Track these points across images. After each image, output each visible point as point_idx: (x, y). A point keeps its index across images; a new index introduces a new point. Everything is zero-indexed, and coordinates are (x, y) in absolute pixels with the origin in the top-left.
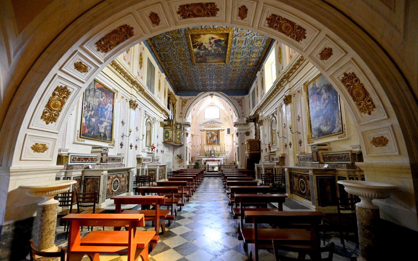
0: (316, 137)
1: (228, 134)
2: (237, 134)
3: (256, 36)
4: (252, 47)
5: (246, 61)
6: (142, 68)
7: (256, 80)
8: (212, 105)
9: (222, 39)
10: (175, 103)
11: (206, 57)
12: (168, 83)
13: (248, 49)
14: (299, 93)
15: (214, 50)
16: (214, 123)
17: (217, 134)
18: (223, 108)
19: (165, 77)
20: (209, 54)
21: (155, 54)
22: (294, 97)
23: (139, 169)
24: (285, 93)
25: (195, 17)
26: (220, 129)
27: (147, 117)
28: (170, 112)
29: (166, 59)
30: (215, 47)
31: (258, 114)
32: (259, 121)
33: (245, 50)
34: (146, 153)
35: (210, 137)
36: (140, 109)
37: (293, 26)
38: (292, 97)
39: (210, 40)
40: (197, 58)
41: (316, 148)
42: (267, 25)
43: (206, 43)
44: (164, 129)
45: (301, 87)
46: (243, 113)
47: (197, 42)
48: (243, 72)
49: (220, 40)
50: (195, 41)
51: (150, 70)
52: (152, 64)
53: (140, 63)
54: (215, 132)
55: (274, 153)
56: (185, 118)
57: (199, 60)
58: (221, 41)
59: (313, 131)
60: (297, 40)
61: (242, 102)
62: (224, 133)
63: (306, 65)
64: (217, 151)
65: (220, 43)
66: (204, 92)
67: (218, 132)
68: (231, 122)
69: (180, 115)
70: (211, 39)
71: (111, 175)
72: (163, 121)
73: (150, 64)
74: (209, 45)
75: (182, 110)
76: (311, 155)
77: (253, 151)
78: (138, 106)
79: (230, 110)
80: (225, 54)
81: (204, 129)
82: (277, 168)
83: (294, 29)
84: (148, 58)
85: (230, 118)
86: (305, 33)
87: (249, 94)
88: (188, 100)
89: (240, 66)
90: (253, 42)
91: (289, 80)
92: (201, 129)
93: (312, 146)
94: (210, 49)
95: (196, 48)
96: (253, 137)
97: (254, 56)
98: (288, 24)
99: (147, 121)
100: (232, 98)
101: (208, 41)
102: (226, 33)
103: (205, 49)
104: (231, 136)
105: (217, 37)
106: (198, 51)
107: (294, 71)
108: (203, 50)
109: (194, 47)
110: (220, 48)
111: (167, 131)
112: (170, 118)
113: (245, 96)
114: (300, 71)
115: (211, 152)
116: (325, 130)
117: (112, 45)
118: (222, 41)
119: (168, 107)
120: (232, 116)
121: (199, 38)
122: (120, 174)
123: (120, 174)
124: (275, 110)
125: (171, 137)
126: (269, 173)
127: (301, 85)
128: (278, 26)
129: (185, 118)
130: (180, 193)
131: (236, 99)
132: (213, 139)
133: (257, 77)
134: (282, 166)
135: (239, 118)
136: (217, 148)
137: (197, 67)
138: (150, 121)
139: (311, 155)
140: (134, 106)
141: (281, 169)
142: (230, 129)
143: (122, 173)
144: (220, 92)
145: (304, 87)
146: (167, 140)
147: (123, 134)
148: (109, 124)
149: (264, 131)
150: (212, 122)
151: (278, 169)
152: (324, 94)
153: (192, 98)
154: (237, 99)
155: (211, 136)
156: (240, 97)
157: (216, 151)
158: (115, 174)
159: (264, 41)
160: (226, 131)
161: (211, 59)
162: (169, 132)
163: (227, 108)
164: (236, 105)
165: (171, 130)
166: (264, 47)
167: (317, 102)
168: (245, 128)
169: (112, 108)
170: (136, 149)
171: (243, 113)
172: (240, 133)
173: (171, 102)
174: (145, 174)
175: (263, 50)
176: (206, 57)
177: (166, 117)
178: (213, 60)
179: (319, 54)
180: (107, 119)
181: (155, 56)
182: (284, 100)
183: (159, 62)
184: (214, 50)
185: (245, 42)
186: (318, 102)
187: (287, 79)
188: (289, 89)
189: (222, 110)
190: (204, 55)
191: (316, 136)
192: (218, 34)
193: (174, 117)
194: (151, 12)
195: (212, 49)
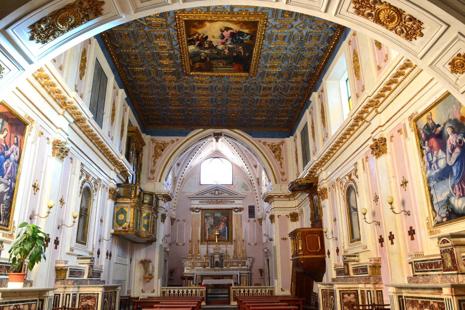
0: (445, 220)
5: (291, 73)
6: (84, 78)
7: (310, 107)
8: (217, 155)
9: (246, 31)
11: (212, 62)
12: (129, 108)
14: (401, 133)
15: (228, 50)
16: (221, 194)
17: (226, 218)
18: (239, 162)
19: (125, 96)
20: (219, 56)
21: (110, 52)
22: (391, 141)
23: (60, 295)
24: (372, 133)
27: (84, 178)
28: (130, 168)
29: (130, 62)
30: (230, 44)
31: (316, 176)
32: (318, 190)
34: (76, 257)
35: (212, 224)
36: (71, 159)
37: (401, 16)
38: (388, 142)
39: (222, 31)
40: (194, 63)
41: (448, 242)
42: (353, 10)
43: (213, 37)
44: (115, 203)
45: (403, 123)
46: (283, 174)
47: (197, 35)
49: (241, 33)
50: (192, 33)
51: (98, 83)
52: (102, 70)
53: (80, 69)
54: (222, 214)
55: (356, 258)
56: (160, 181)
57: (197, 66)
58: (244, 35)
59: (436, 208)
60: (408, 39)
61: (280, 150)
62: (241, 215)
63: (409, 84)
65: (241, 38)
66: (201, 130)
67: (227, 212)
68: (257, 191)
69: (150, 175)
70: (225, 30)
71: (6, 303)
72: (115, 187)
73: (99, 72)
74: (220, 40)
75: (154, 165)
76: (440, 257)
77: (310, 253)
78: (69, 153)
79: (254, 168)
80: (250, 57)
81: (199, 206)
82: (366, 290)
83: (401, 20)
84: (97, 59)
85: (255, 185)
86: (421, 28)
87: (294, 135)
88: (168, 144)
91: (379, 110)
92: (192, 206)
93: (439, 238)
94: (220, 47)
95: (195, 44)
96: (305, 222)
97: (305, 63)
98: (391, 12)
99: (82, 185)
100: (260, 142)
101: (218, 34)
103: (211, 46)
105: (235, 28)
106: (197, 50)
107: (387, 93)
108: (206, 49)
109: (191, 42)
110: (240, 47)
112: (130, 181)
113: (286, 139)
114: (400, 93)
116: (460, 205)
117: (60, 30)
118: (246, 35)
119: (128, 157)
121: (201, 28)
122: (24, 301)
123: (24, 301)
124: (353, 167)
126: (350, 302)
127: (405, 119)
128: (373, 13)
129: (160, 181)
130: (343, 269)
131: (269, 145)
133: (311, 102)
134: (377, 286)
135: (276, 183)
136: (228, 249)
138: (89, 186)
139: (440, 257)
140: (62, 152)
141: (375, 293)
143: (28, 301)
145: (410, 124)
146: (120, 228)
147: (33, 212)
148: (8, 189)
149: (333, 209)
150: (217, 193)
151: (368, 291)
152: (450, 136)
153: (177, 140)
154: (270, 144)
155: (214, 223)
156: (276, 141)
158: (13, 302)
160: (245, 213)
163: (249, 164)
164: (269, 156)
167: (438, 151)
169: (18, 154)
170: (56, 248)
171: (283, 174)
172: (279, 216)
173: (134, 148)
174: (72, 305)
176: (212, 62)
177: (122, 178)
178: (225, 67)
179: (448, 63)
180: (5, 177)
181: (111, 56)
182: (371, 147)
183: (116, 67)
184: (229, 49)
186: (440, 151)
187: (375, 108)
188: (380, 126)
189: (237, 166)
190: (208, 59)
191: (444, 217)
192: (236, 23)
193: (138, 180)
195: (226, 48)
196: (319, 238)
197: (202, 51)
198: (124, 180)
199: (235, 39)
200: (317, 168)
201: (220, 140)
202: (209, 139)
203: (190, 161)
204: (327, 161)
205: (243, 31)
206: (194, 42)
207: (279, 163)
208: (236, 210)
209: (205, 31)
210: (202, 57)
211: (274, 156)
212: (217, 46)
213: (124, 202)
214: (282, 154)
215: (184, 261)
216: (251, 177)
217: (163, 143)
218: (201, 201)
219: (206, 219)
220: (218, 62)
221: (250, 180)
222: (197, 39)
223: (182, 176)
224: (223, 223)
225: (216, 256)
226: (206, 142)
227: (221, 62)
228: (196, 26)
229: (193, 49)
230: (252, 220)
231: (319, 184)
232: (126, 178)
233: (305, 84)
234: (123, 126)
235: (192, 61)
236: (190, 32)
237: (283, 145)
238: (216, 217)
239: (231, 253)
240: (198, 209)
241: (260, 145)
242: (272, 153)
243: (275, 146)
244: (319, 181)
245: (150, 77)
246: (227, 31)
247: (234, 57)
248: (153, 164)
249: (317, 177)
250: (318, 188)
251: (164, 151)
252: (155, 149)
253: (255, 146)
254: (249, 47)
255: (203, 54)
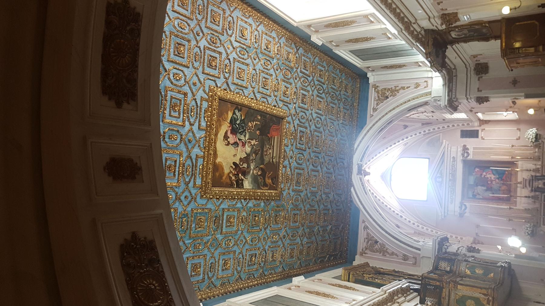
1: (477, 137)
2: (481, 100)
3: (233, 39)
4: (255, 50)
8: (385, 177)
9: (230, 114)
10: (373, 268)
11: (265, 162)
12: (318, 276)
13: (257, 60)
15: (252, 140)
17: (477, 170)
19: (302, 278)
20: (259, 152)
25: (137, 67)
26: (460, 158)
31: (423, 32)
33: (259, 67)
35: (485, 188)
39: (228, 144)
47: (231, 175)
48: (310, 79)
49: (233, 122)
52: (266, 299)
56: (419, 250)
58: (235, 118)
61: (385, 89)
62: (474, 148)
64: (536, 170)
65: (238, 122)
66: (352, 189)
74: (240, 148)
75: (396, 255)
79: (407, 129)
84: (251, 303)
87: (365, 70)
88: (368, 234)
89: (294, 84)
90: (245, 47)
94: (248, 149)
95: (242, 180)
96: (491, 49)
102: (219, 103)
103: (246, 160)
104: (487, 127)
105: (225, 127)
106: (249, 177)
108: (249, 167)
109: (240, 184)
111: (458, 301)
112: (416, 287)
115: (537, 189)
120: (423, 124)
121: (223, 169)
125: (479, 290)
129: (419, 250)
131: (377, 104)
132: (492, 181)
137: (287, 190)
142: (462, 131)
144: (356, 146)
153: (364, 222)
154: (376, 102)
155: (482, 186)
156: (372, 95)
157: (533, 174)
159: (246, 22)
160: (471, 143)
161: (271, 151)
162: (460, 294)
165: (456, 287)
166: (257, 24)
168: (461, 76)
172: (479, 90)
175: (265, 26)
176: (265, 162)
178: (273, 146)
184: (251, 139)
185: (243, 63)
194: (104, 169)
196: (518, 24)
197: (251, 172)
198: (415, 294)
199: (240, 129)
200: (412, 29)
201: (367, 170)
202: (367, 185)
203: (394, 212)
204: (403, 13)
205: (230, 118)
206: (240, 180)
207: (401, 91)
208: (466, 155)
209: (227, 165)
210: (259, 173)
211: (392, 97)
212: (246, 153)
213: (447, 298)
214: (390, 87)
215: (542, 230)
216: (420, 133)
217: (366, 240)
218: (450, 201)
219: (478, 197)
220: (266, 155)
221: (424, 135)
222: (236, 175)
223: (414, 224)
224: (484, 173)
225: (536, 184)
226: (369, 188)
227: (266, 151)
228: (220, 174)
229: (249, 183)
230: (481, 134)
231: (435, 28)
232: (411, 291)
233: (300, 52)
234: (340, 286)
235: (263, 187)
236: (227, 183)
237: (378, 86)
238: (475, 182)
239: (531, 165)
240: (462, 206)
241: (377, 115)
242: (388, 99)
243: (378, 97)
244: (431, 27)
245: (280, 243)
246: (229, 138)
247: (261, 134)
248: (394, 256)
249: (425, 31)
250: (440, 28)
251: (378, 240)
252: (374, 252)
253: (377, 122)
254: (251, 113)
255: (255, 172)
